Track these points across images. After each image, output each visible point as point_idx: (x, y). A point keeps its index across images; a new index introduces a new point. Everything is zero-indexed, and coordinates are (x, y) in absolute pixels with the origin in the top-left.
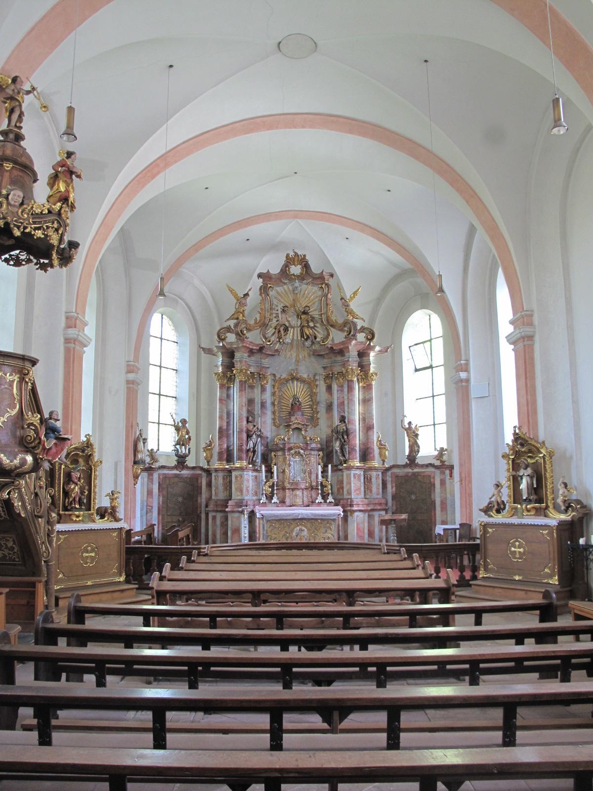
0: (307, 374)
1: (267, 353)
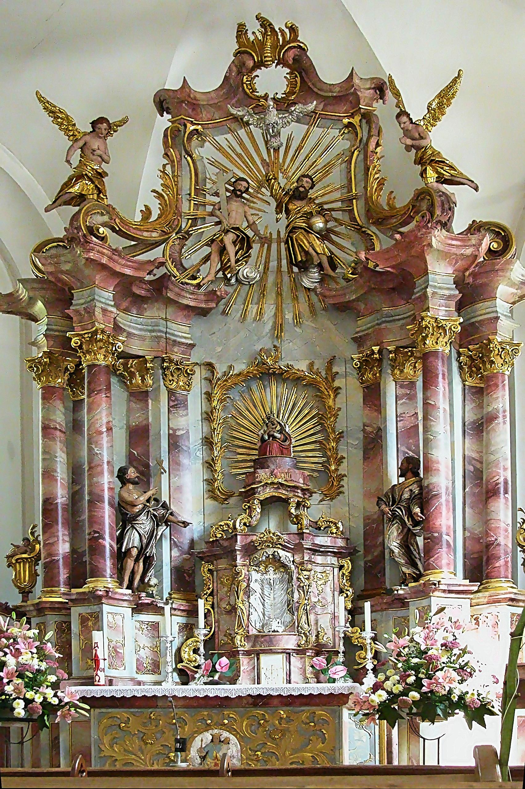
0: (307, 362)
1: (185, 302)
